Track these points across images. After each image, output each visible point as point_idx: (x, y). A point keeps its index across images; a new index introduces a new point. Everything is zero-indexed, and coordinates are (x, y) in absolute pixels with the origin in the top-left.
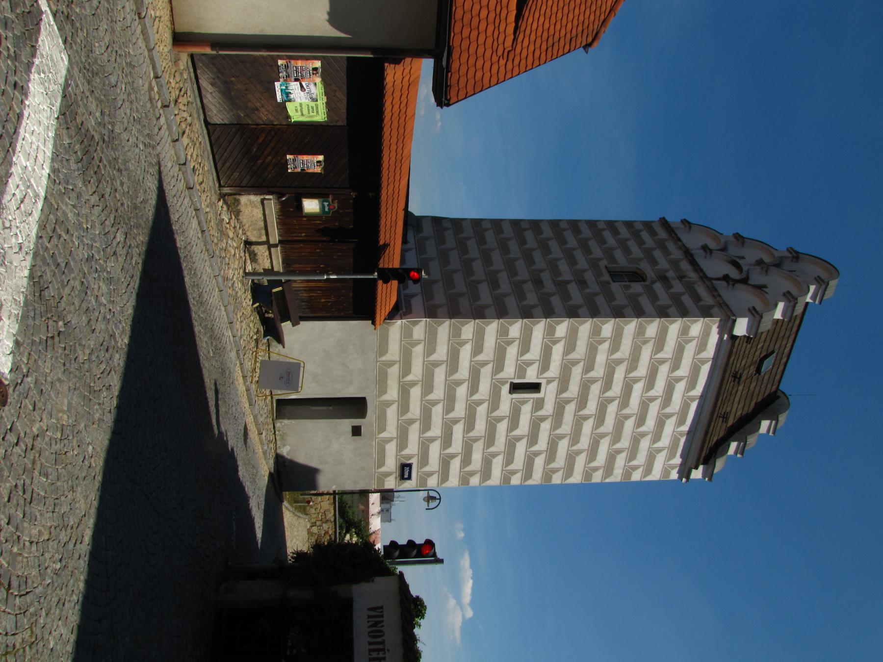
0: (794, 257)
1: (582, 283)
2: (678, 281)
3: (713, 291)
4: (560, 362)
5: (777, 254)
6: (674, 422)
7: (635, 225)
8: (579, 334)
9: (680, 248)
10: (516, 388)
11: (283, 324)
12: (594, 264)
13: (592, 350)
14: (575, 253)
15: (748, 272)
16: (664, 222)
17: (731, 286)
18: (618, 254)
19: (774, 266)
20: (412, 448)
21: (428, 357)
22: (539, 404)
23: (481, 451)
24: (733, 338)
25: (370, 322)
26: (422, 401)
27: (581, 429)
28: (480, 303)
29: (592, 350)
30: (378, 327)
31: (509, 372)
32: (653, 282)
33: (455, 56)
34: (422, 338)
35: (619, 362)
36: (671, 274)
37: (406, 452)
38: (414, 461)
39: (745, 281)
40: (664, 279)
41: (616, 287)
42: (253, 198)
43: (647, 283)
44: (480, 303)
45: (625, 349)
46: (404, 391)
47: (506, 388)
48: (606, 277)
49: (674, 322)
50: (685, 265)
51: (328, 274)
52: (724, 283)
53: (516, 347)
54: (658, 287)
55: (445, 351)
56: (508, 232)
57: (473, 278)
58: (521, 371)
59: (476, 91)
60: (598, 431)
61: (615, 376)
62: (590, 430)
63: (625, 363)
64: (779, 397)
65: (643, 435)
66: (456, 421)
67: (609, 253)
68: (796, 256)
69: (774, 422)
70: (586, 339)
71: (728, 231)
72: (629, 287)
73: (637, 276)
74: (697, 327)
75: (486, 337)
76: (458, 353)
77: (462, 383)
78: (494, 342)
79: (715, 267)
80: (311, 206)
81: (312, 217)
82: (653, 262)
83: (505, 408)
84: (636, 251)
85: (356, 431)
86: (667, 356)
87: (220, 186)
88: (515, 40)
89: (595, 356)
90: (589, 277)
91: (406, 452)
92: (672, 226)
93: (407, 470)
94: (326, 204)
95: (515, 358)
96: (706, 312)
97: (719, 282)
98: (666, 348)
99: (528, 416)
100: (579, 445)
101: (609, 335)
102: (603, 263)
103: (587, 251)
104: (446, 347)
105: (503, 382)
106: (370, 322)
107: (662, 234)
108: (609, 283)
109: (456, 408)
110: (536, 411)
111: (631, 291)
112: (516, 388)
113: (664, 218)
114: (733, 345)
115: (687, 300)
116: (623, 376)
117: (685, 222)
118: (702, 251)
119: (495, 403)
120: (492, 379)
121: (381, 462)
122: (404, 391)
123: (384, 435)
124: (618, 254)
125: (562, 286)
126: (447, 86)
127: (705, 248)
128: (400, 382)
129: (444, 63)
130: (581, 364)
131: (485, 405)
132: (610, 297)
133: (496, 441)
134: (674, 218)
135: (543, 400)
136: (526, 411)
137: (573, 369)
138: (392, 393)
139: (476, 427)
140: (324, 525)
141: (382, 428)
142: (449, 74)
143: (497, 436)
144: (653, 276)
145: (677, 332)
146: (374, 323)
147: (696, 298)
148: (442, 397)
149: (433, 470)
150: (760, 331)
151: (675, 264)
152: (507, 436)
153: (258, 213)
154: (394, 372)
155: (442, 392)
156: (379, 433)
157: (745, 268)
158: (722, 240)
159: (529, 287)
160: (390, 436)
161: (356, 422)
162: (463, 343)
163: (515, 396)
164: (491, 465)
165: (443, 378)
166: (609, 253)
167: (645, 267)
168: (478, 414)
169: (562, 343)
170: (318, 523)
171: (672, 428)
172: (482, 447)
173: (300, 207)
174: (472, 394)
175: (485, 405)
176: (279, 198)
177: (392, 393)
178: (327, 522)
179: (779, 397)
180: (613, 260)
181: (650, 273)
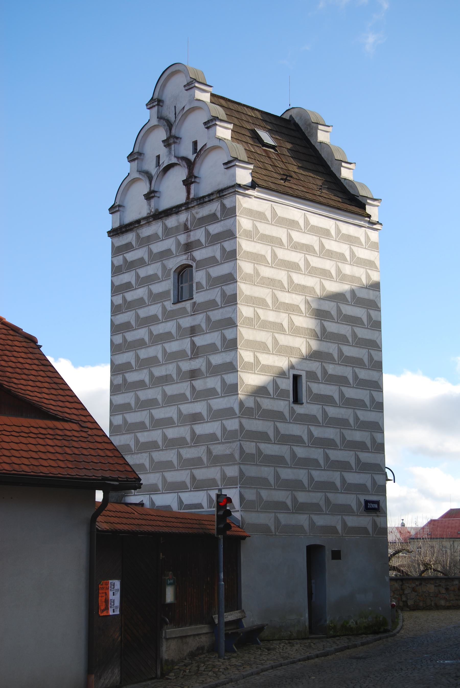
0: (158, 105)
1: (194, 331)
2: (192, 233)
3: (202, 201)
4: (275, 356)
5: (155, 122)
6: (328, 241)
7: (116, 264)
8: (251, 338)
9: (149, 223)
10: (297, 400)
11: (245, 626)
12: (169, 316)
13: (265, 325)
14: (155, 333)
15: (178, 158)
16: (113, 233)
17: (197, 180)
18: (157, 288)
19: (170, 130)
20: (351, 500)
21: (271, 486)
22: (311, 375)
23: (354, 432)
24: (253, 185)
25: (242, 541)
26: (309, 491)
27: (333, 334)
28: (219, 434)
29: (265, 325)
30: (248, 534)
31: (282, 406)
32: (193, 259)
33: (107, 475)
34: (254, 491)
35: (275, 298)
36: (182, 238)
37: (354, 507)
38: (362, 498)
39: (190, 165)
40: (188, 247)
41: (199, 297)
42: (164, 648)
43: (194, 265)
44: (219, 434)
45: (263, 293)
46: (300, 508)
47: (299, 409)
48: (188, 305)
49: (240, 246)
50: (172, 222)
51: (219, 580)
52: (193, 187)
53: (262, 399)
54: (199, 254)
55: (266, 469)
56: (127, 398)
57: (188, 439)
58: (281, 394)
59: (121, 456)
60: (335, 316)
61: (287, 302)
62: (334, 324)
63: (276, 292)
64: (291, 116)
65: (339, 271)
66: (327, 457)
67: (156, 298)
68: (156, 102)
69: (343, 164)
70: (255, 332)
71: (125, 168)
72: (198, 284)
73: (183, 273)
74: (244, 223)
75: (254, 429)
76: (268, 456)
77: (294, 452)
78: (258, 422)
79: (173, 191)
80: (170, 595)
81: (177, 595)
82: (166, 254)
83: (314, 409)
84: (153, 269)
85: (336, 555)
86: (269, 251)
87: (156, 678)
88: (70, 421)
89: (270, 322)
90: (186, 322)
91: (354, 507)
92: (117, 225)
93: (370, 505)
94: (169, 582)
95: (272, 401)
96: (230, 213)
97: (192, 192)
98: (263, 253)
99: (322, 386)
100: (348, 335)
101: (252, 309)
102: (169, 305)
103: (153, 320)
104: (263, 468)
105: (292, 411)
106: (242, 541)
107: (130, 237)
108: (195, 303)
109: (315, 457)
110: (317, 378)
111: (204, 283)
112: (297, 400)
113: (109, 232)
114: (259, 186)
115: (215, 229)
116: (287, 294)
117: (113, 209)
118: (153, 201)
119: (309, 420)
120: (290, 423)
121: (364, 530)
122: (300, 508)
123: (339, 528)
124: (157, 288)
125: (196, 352)
126: (127, 481)
127: (149, 196)
128: (293, 513)
129: (116, 483)
130: (276, 335)
131: (312, 428)
132: (211, 305)
133: (345, 417)
134: (108, 222)
135: (307, 372)
136: (317, 388)
137: (281, 343)
138: (302, 519)
139: (332, 437)
140: (406, 592)
141: (333, 530)
142: (120, 479)
143: (340, 417)
144: (185, 257)
145: (248, 243)
146: (244, 538)
147: (212, 218)
148: (305, 471)
149: (370, 479)
150: (247, 161)
151: (168, 232)
152: (340, 407)
153: (173, 645)
154: (284, 518)
155: (302, 471)
156: (337, 532)
157: (174, 160)
158: (137, 175)
159: (199, 384)
160: (340, 522)
161: (328, 555)
162: (259, 450)
163: (304, 400)
164: (365, 422)
165: (289, 470)
166: (156, 298)
167: (174, 263)
168: (320, 436)
169: (259, 355)
170: (404, 599)
171: (333, 242)
172: (350, 432)
173: (170, 605)
174: (302, 441)
175: (312, 428)
176: (167, 624)
177: (302, 519)
178: (403, 590)
179: (291, 116)
180: (162, 296)
181: (182, 260)
